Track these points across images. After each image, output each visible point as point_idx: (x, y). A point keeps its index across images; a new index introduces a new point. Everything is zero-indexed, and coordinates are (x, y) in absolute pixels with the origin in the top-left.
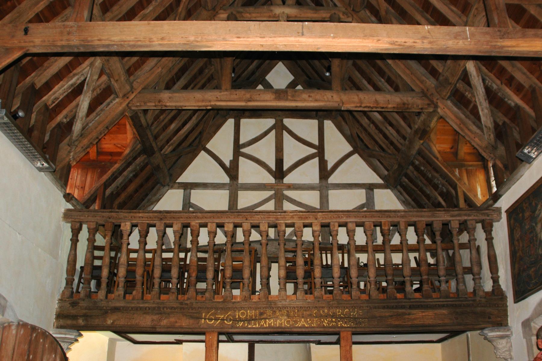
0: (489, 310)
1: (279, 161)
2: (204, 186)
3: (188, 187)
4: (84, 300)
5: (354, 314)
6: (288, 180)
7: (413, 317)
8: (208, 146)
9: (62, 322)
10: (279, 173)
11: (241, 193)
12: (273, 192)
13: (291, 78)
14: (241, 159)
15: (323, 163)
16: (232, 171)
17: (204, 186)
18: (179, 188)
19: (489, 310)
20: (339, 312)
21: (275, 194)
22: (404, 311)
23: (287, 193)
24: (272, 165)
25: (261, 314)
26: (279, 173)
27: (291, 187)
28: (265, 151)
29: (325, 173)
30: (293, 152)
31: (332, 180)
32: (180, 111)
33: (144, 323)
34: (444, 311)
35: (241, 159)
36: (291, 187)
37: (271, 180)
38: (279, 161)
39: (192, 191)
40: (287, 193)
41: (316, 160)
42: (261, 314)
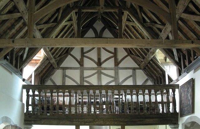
0: (172, 119)
1: (99, 59)
2: (71, 68)
3: (65, 69)
4: (33, 115)
5: (126, 120)
6: (104, 65)
7: (145, 121)
8: (71, 53)
9: (26, 122)
10: (99, 63)
11: (85, 71)
12: (96, 71)
13: (103, 25)
14: (85, 59)
15: (116, 60)
16: (81, 63)
17: (71, 68)
18: (61, 69)
19: (172, 119)
20: (120, 119)
21: (97, 72)
22: (142, 119)
23: (103, 71)
24: (96, 60)
25: (94, 120)
26: (99, 63)
27: (105, 69)
28: (93, 55)
29: (117, 63)
30: (105, 55)
31: (121, 65)
32: (58, 48)
33: (9, 16)
34: (157, 119)
35: (85, 59)
36: (105, 69)
37: (95, 66)
38: (99, 59)
39: (66, 70)
40: (103, 71)
41: (113, 58)
42: (94, 120)
